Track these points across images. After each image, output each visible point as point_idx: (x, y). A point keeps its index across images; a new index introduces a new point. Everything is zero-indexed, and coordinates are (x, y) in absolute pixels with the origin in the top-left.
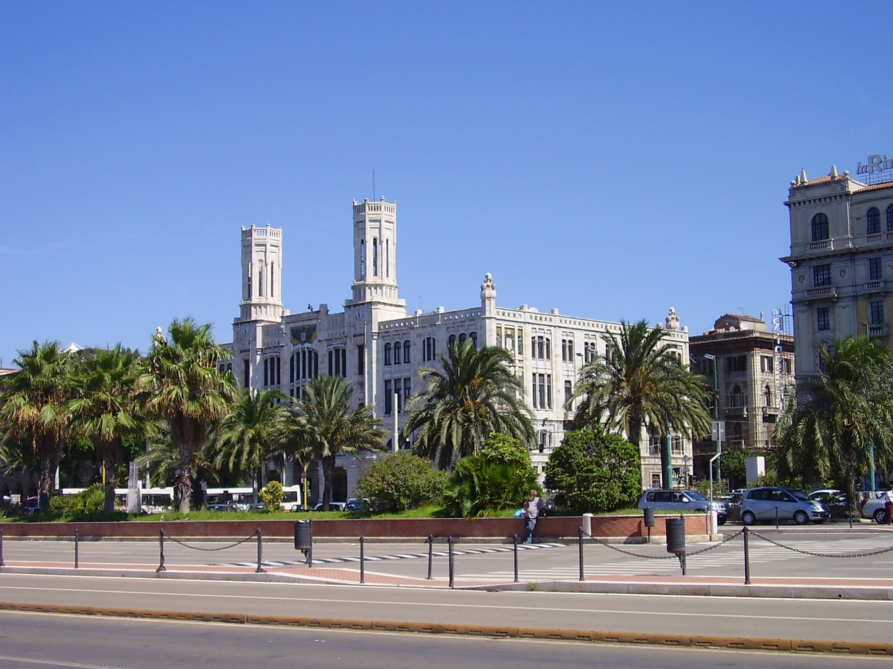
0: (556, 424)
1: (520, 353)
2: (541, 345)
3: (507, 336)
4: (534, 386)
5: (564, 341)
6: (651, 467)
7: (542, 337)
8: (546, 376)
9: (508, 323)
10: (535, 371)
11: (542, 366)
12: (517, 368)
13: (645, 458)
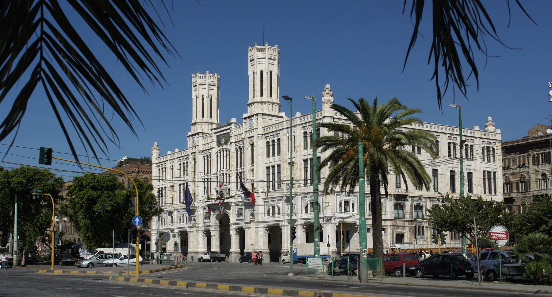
2: (488, 151)
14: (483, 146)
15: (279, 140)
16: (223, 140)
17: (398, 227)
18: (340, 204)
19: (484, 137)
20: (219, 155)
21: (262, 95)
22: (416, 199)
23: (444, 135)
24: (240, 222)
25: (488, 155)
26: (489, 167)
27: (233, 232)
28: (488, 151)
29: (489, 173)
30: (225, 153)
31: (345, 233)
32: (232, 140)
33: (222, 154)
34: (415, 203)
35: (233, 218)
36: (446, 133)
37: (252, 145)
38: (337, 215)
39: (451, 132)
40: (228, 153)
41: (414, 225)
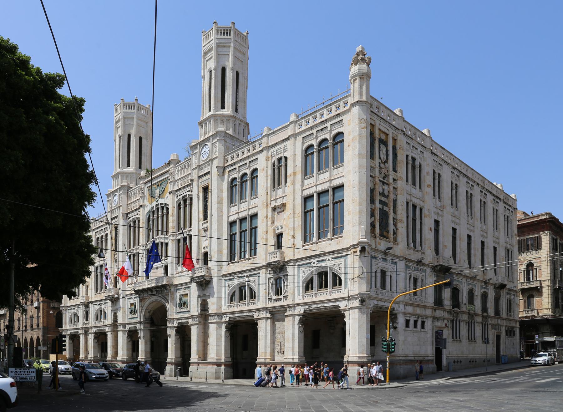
27: (172, 333)
32: (170, 188)
33: (160, 213)
40: (165, 211)
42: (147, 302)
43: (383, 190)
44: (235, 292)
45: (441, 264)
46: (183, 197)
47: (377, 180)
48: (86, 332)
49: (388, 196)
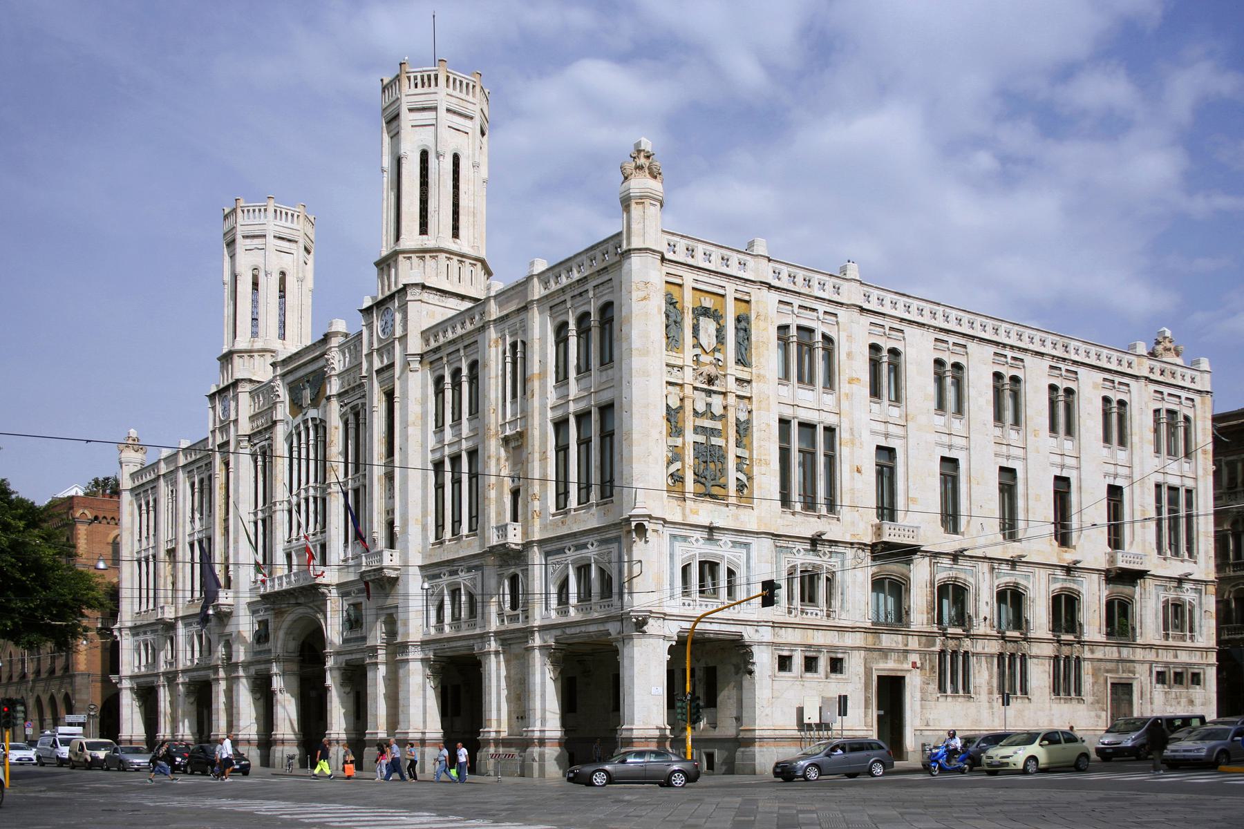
0: (850, 553)
1: (738, 362)
2: (1172, 426)
3: (701, 312)
4: (785, 454)
5: (1053, 388)
6: (1110, 666)
7: (811, 331)
8: (820, 432)
9: (703, 277)
10: (788, 413)
11: (810, 404)
12: (731, 399)
13: (1093, 644)
14: (1158, 405)
15: (474, 366)
16: (307, 394)
17: (885, 653)
18: (685, 570)
19: (1161, 379)
20: (295, 444)
21: (424, 229)
22: (946, 562)
23: (1037, 359)
24: (353, 646)
25: (1172, 434)
26: (1176, 472)
28: (1172, 426)
29: (1173, 490)
30: (312, 433)
31: (699, 674)
34: (941, 576)
35: (334, 631)
36: (1042, 354)
37: (390, 396)
38: (675, 606)
39: (1059, 352)
41: (937, 648)
42: (289, 619)
43: (709, 405)
44: (567, 579)
45: (884, 539)
46: (352, 408)
47: (688, 390)
48: (515, 643)
49: (723, 416)
